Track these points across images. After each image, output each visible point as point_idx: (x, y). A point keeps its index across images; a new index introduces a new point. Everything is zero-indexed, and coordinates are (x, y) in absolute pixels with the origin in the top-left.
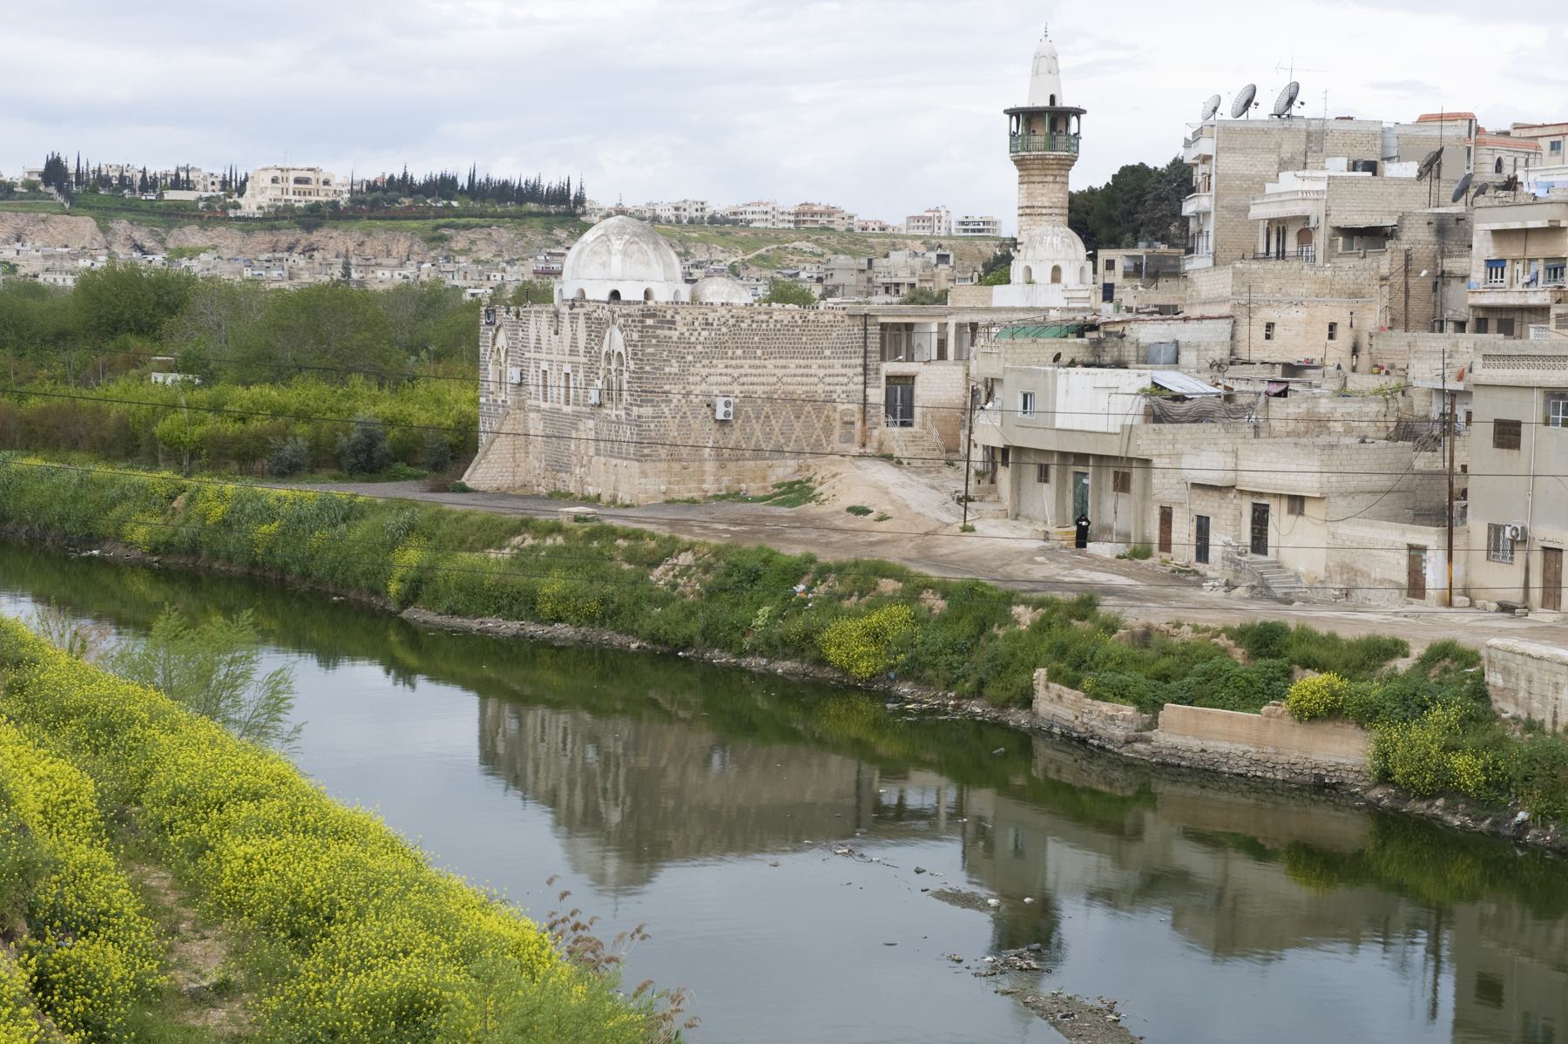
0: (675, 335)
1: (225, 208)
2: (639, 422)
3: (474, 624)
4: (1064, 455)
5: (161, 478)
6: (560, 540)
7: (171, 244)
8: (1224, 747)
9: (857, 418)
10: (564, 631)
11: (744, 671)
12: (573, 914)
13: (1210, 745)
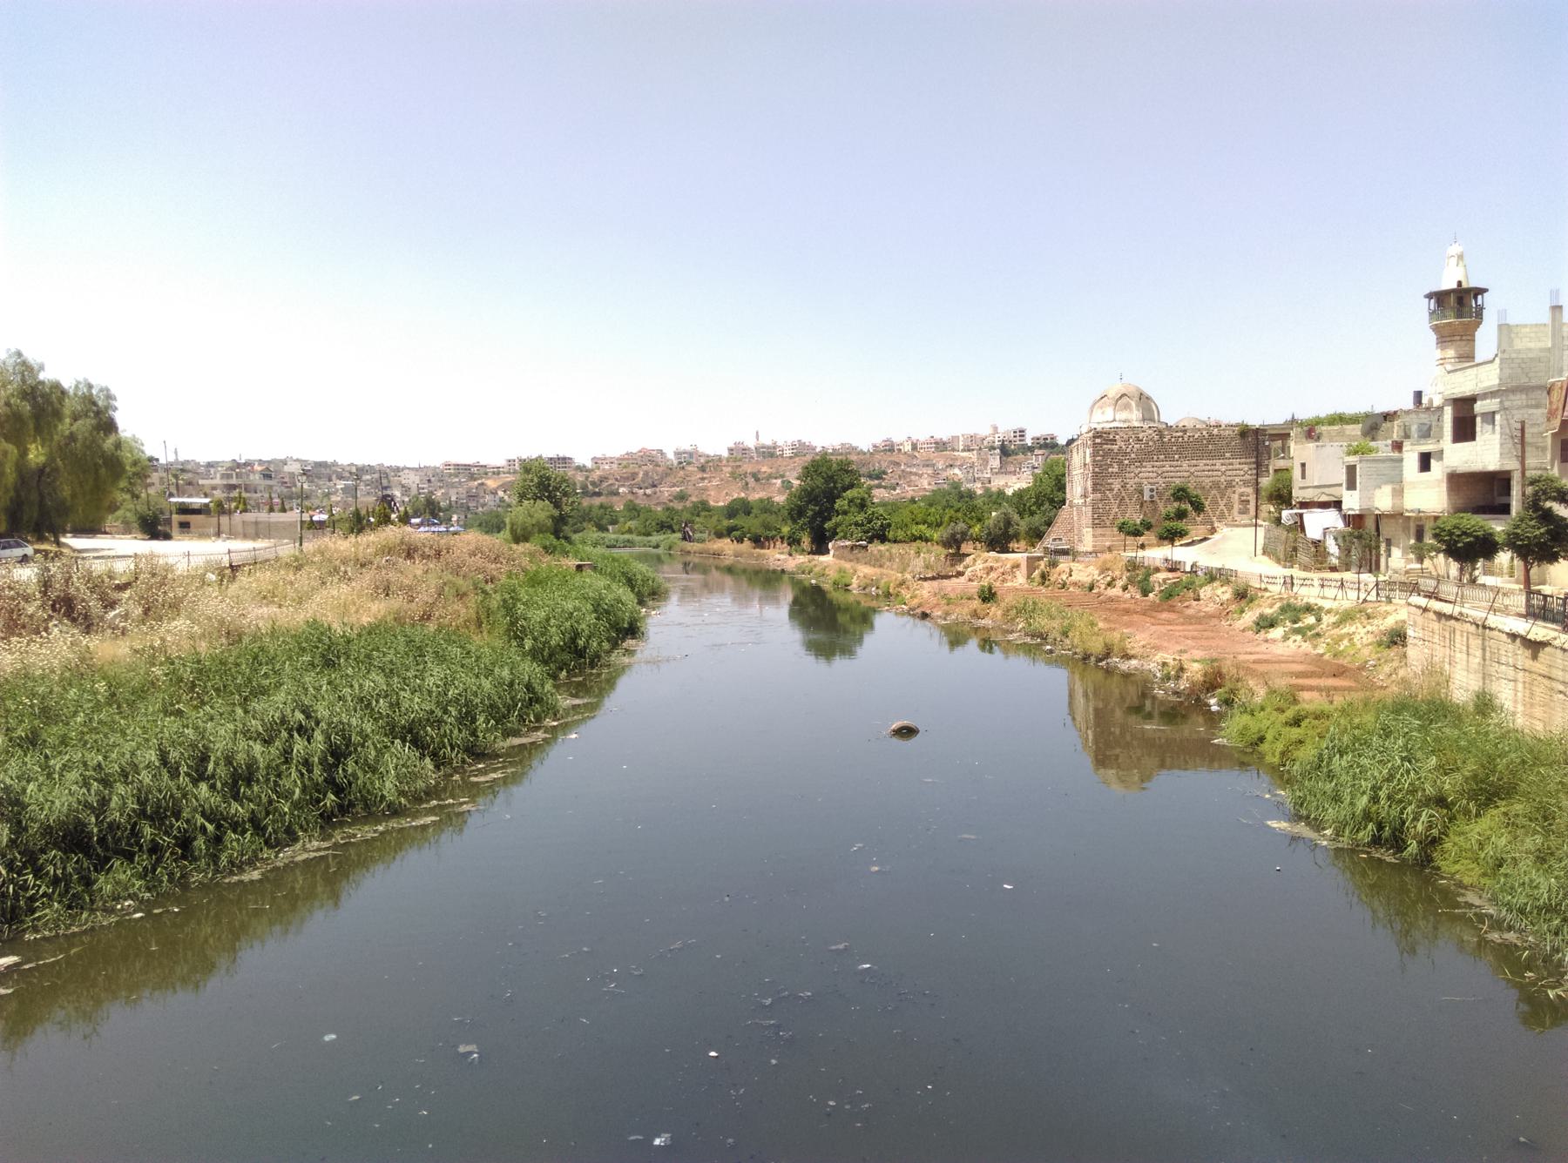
12: (1294, 849)
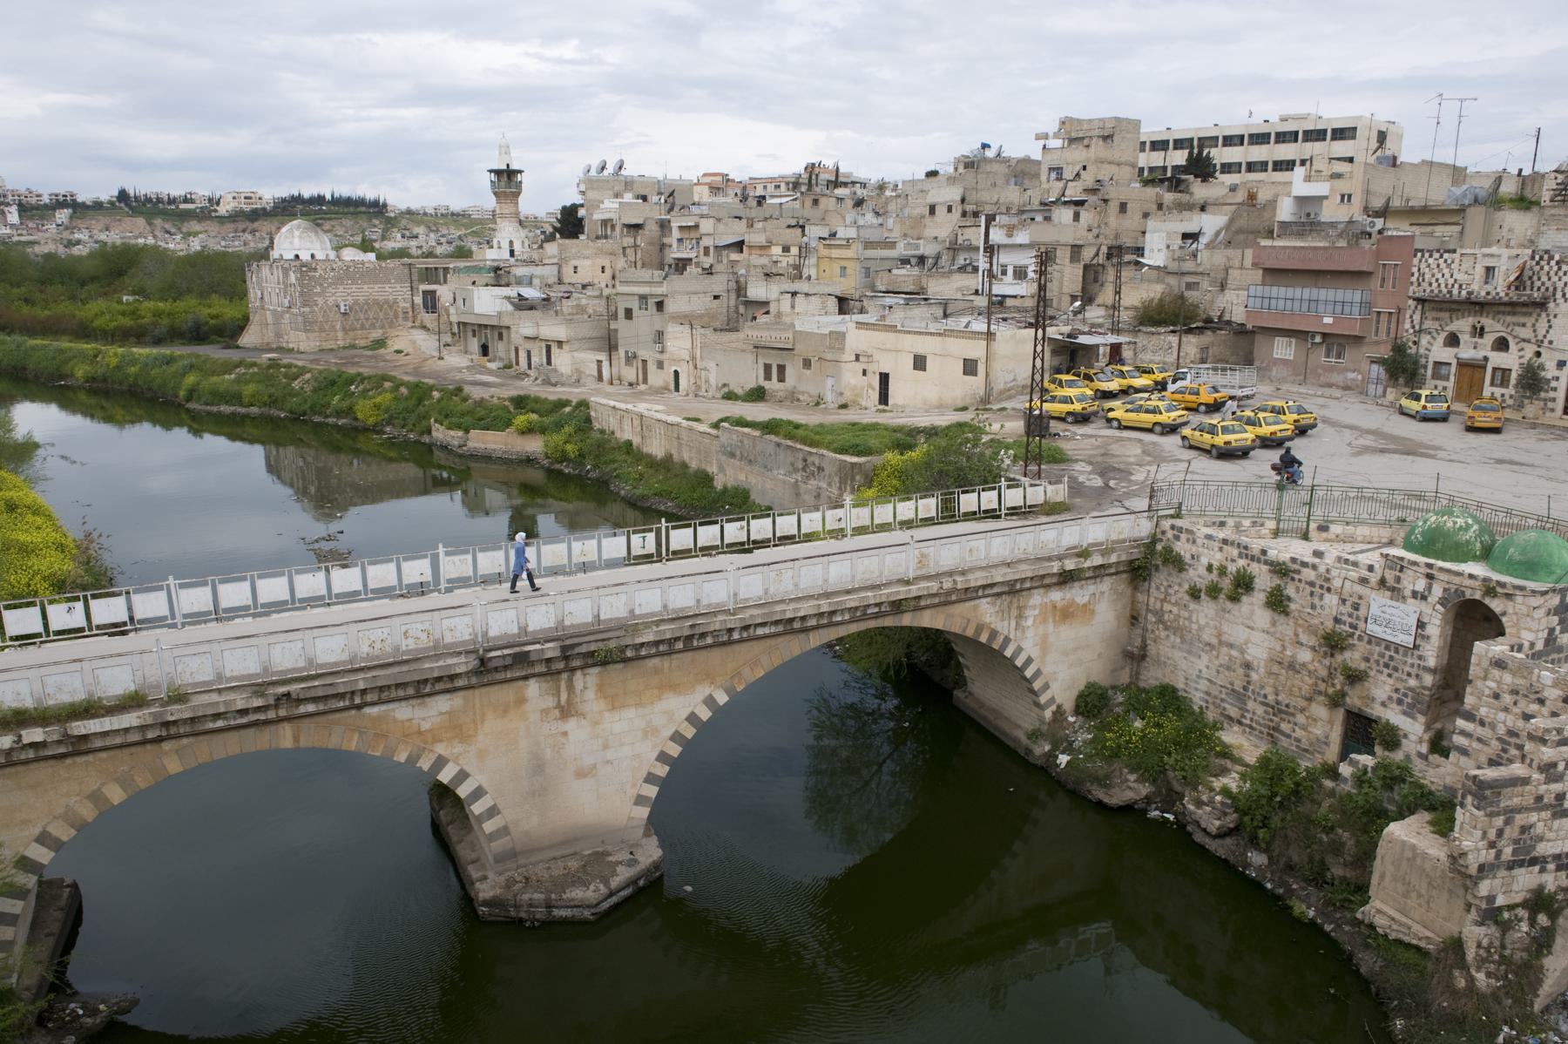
0: (317, 275)
1: (210, 212)
2: (303, 315)
3: (215, 409)
4: (480, 325)
5: (87, 347)
6: (256, 370)
7: (184, 230)
8: (493, 446)
9: (410, 310)
10: (254, 410)
11: (327, 424)
13: (488, 446)
